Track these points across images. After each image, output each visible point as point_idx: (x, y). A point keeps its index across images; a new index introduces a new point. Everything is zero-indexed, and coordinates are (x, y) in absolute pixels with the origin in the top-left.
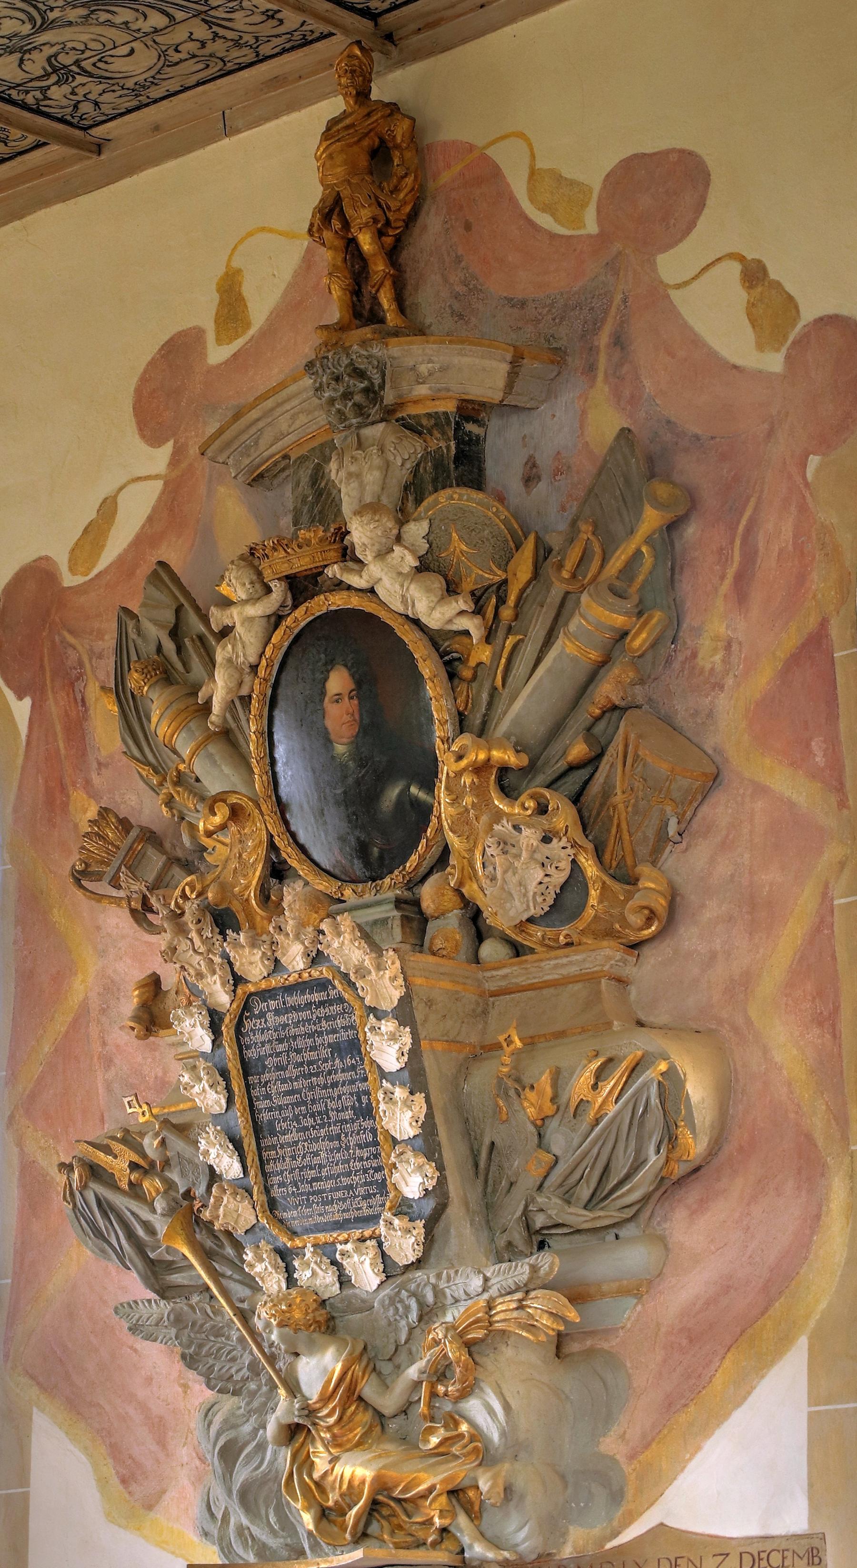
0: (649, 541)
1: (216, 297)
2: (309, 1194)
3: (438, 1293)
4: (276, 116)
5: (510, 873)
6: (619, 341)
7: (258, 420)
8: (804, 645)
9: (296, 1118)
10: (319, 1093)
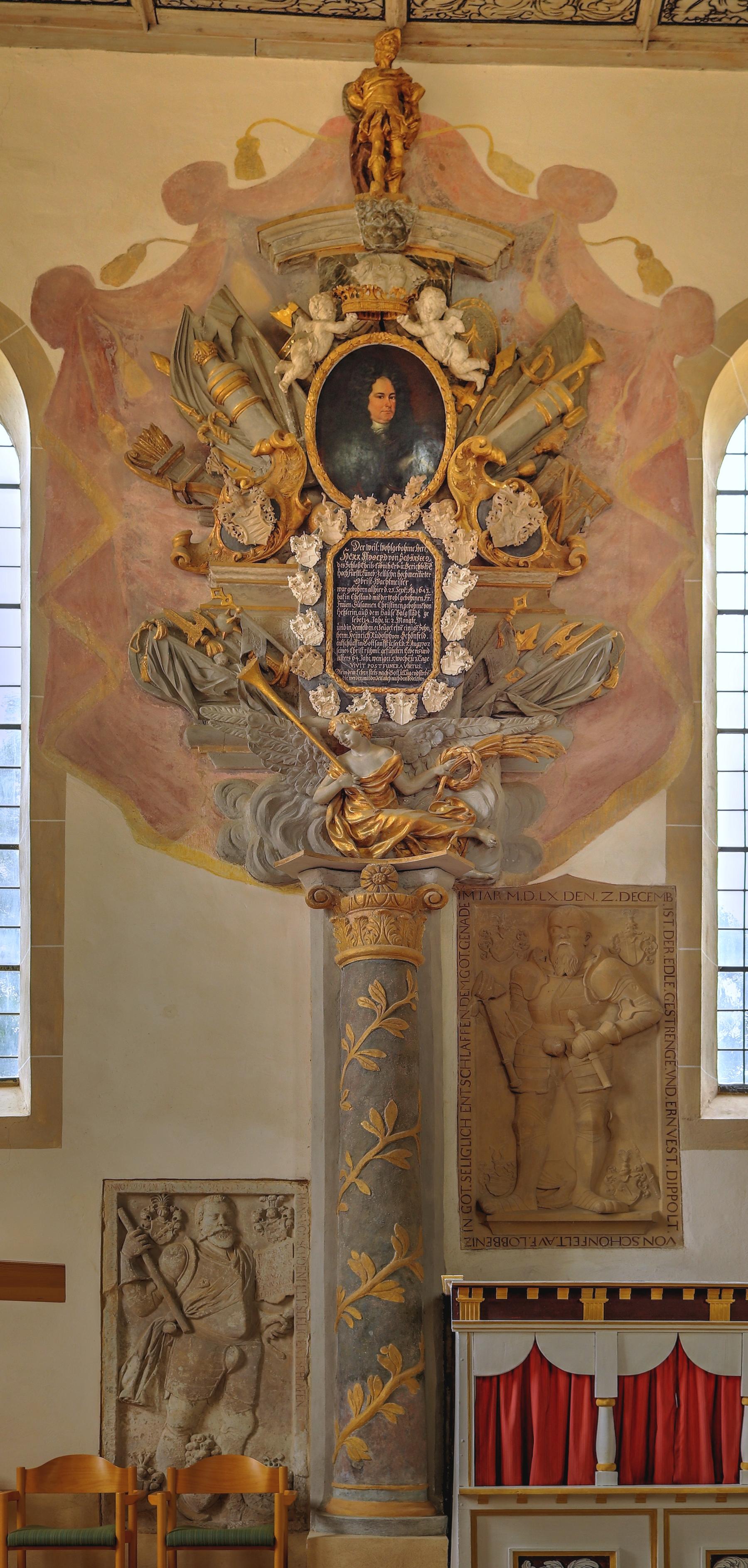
0: (583, 369)
1: (236, 151)
2: (368, 662)
3: (458, 731)
4: (298, 56)
5: (508, 517)
6: (549, 261)
7: (306, 225)
8: (667, 450)
9: (370, 618)
10: (391, 605)
